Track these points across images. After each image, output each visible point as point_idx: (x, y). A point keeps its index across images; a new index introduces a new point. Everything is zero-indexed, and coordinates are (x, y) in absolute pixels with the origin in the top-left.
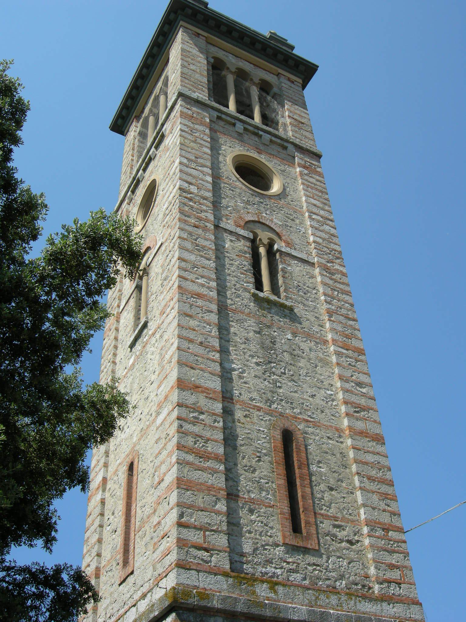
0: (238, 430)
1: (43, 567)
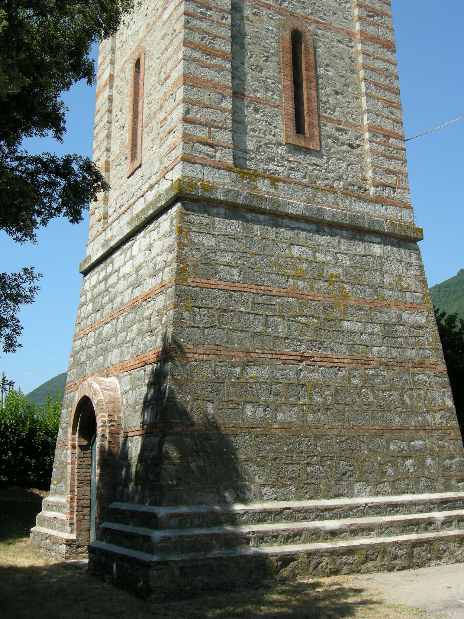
0: (247, 28)
1: (53, 157)
